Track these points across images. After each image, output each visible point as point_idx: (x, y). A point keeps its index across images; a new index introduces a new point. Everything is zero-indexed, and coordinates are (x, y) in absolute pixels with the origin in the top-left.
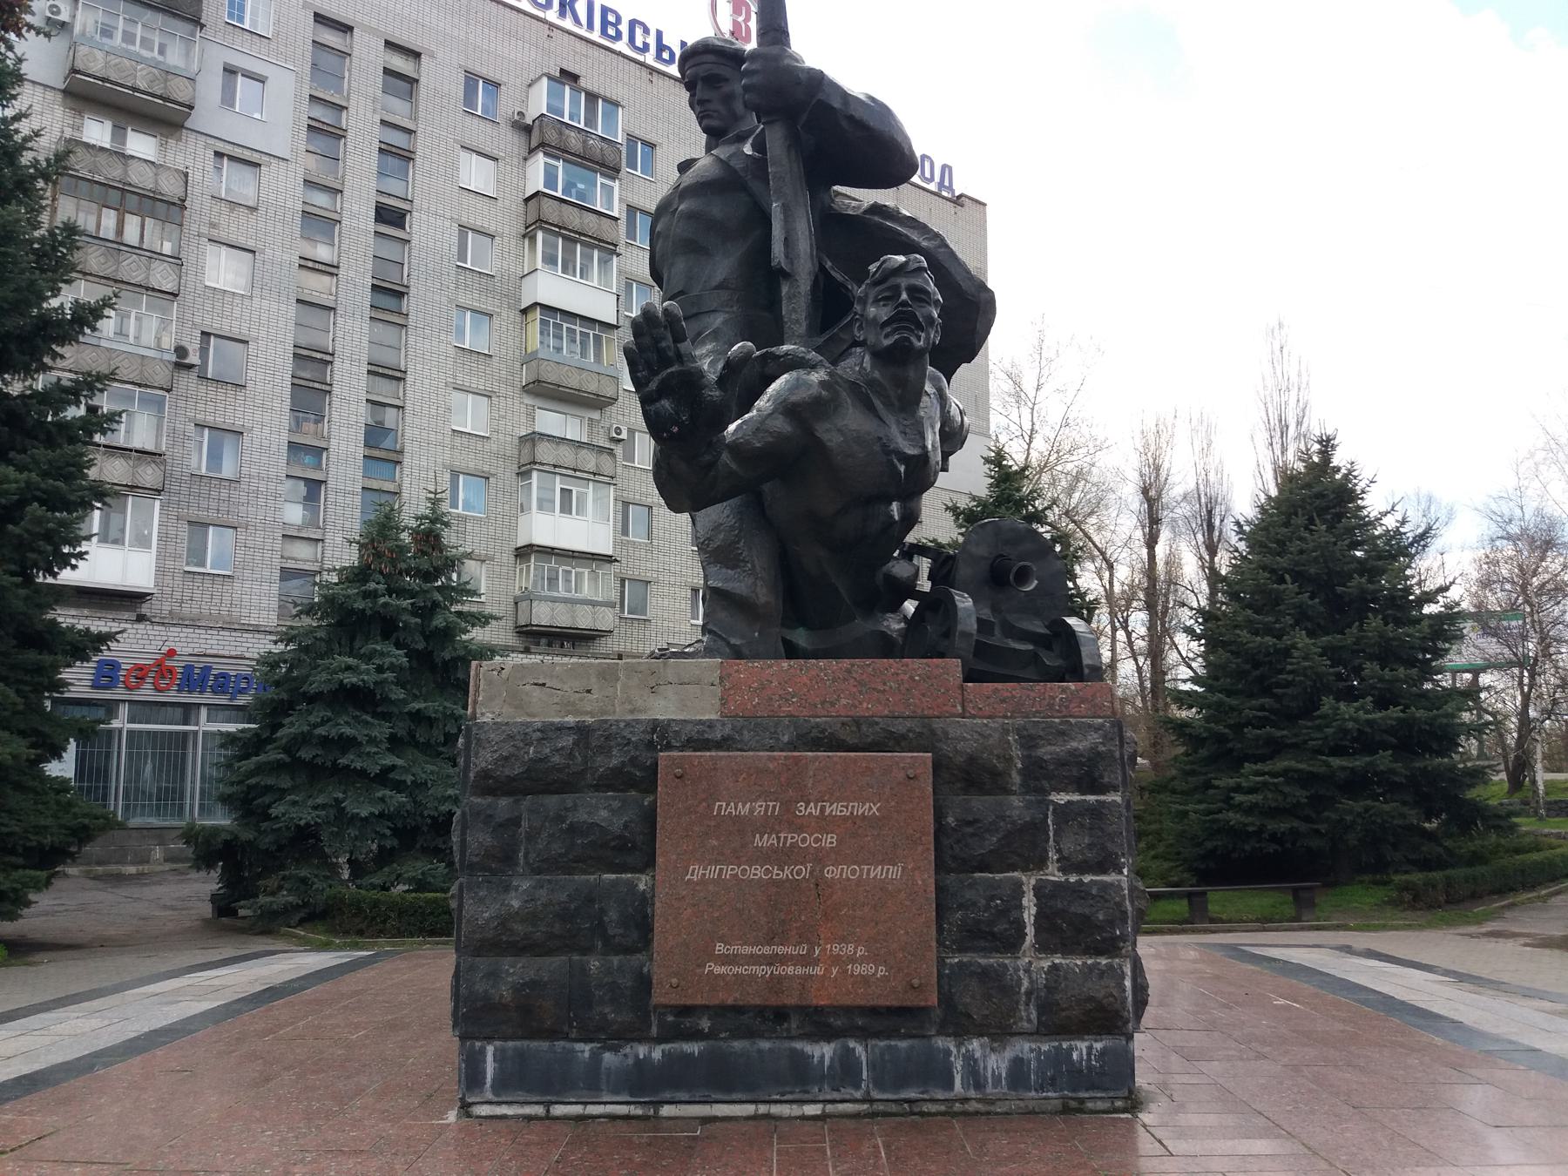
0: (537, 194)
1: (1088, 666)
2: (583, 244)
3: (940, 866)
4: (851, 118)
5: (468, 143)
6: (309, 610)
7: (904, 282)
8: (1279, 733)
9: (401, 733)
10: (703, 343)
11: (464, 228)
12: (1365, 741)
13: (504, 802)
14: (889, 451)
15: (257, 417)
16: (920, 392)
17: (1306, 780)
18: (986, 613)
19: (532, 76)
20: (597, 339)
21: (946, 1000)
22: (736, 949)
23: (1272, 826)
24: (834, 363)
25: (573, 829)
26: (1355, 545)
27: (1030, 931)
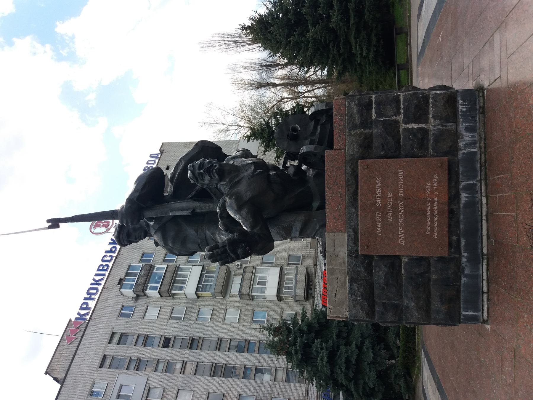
0: (159, 293)
1: (326, 107)
2: (176, 277)
3: (398, 157)
4: (142, 189)
5: (142, 316)
6: (301, 373)
7: (197, 171)
8: (342, 41)
9: (344, 342)
10: (216, 238)
11: (171, 318)
12: (345, 12)
13: (377, 308)
14: (253, 175)
15: (234, 389)
16: (233, 165)
17: (358, 31)
18: (307, 142)
19: (120, 294)
20: (207, 272)
21: (445, 154)
22: (428, 228)
23: (374, 43)
24: (223, 194)
25: (387, 284)
26: (278, 17)
27: (421, 126)
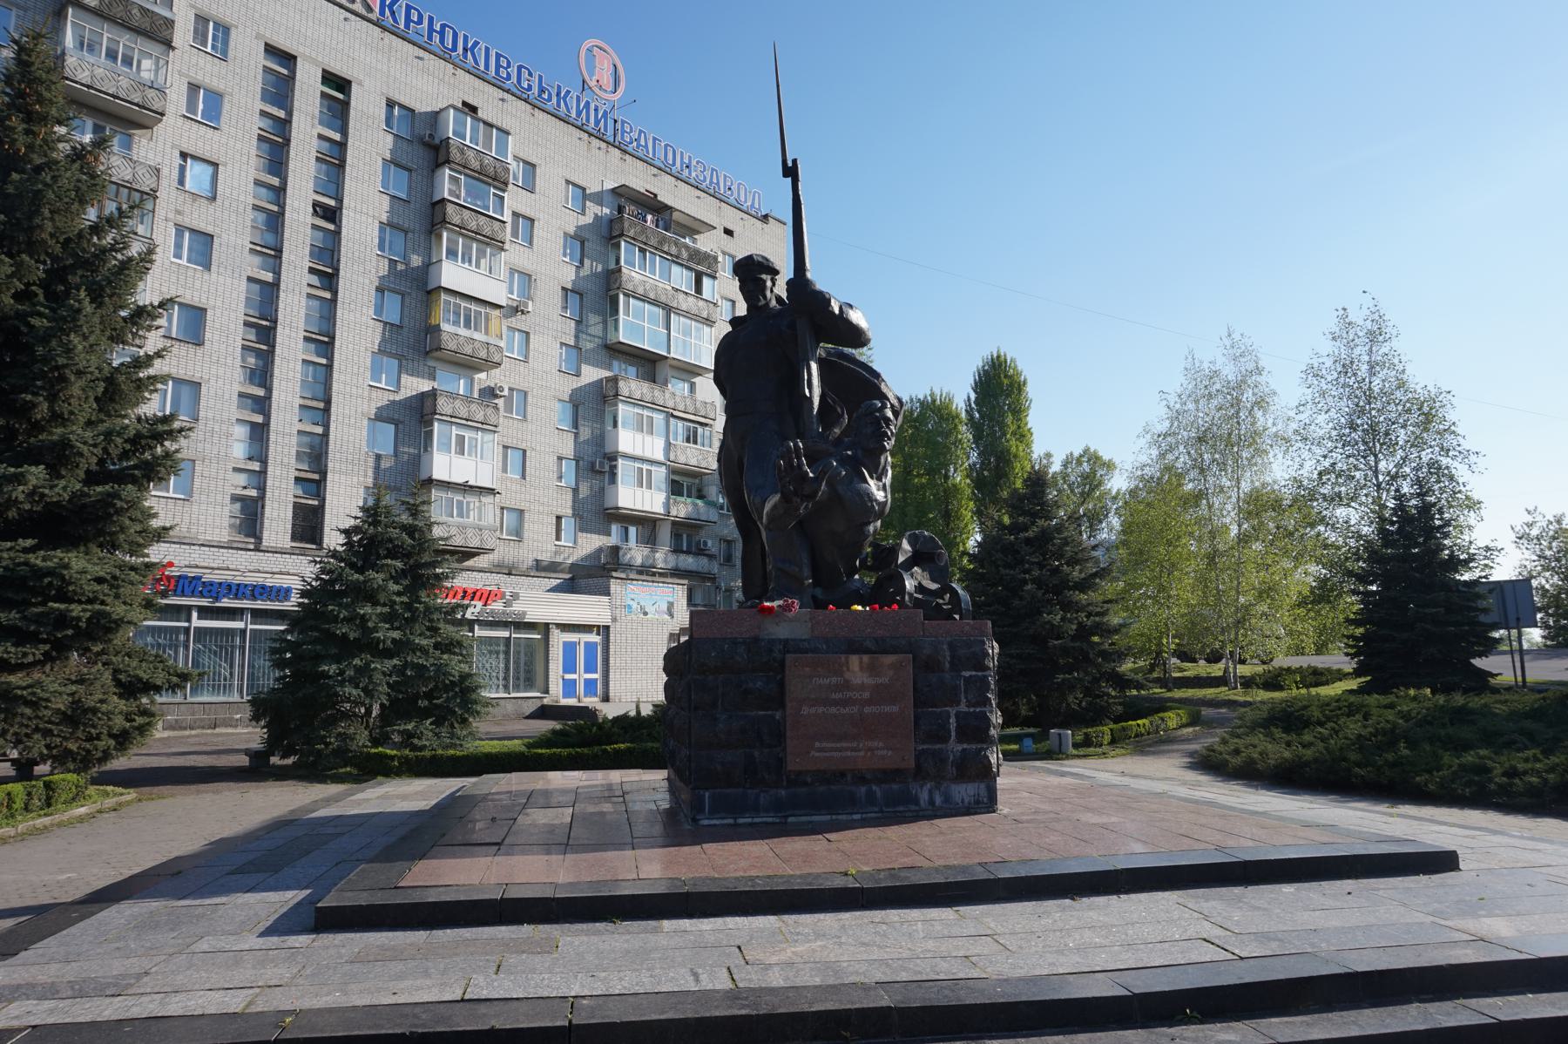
3: (915, 706)
15: (213, 371)
21: (918, 766)
22: (824, 745)
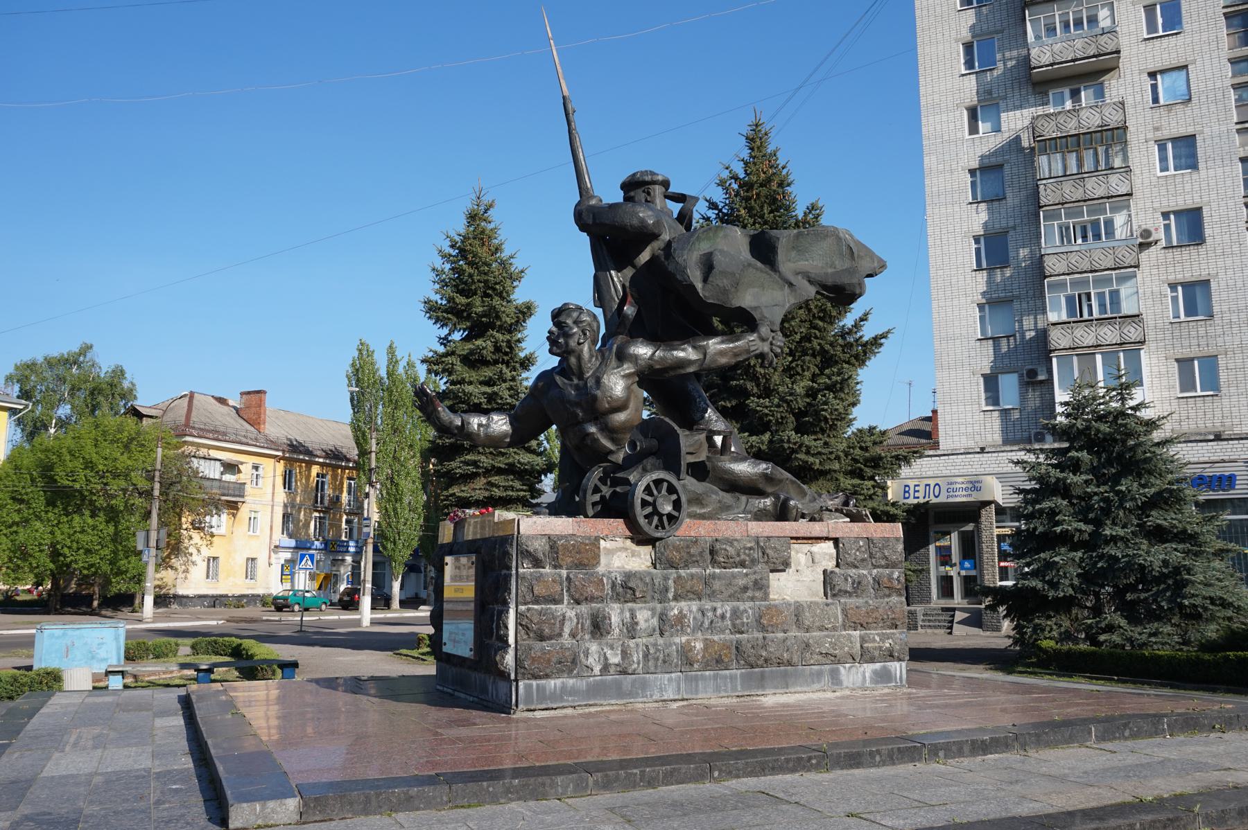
15: (1220, 264)
